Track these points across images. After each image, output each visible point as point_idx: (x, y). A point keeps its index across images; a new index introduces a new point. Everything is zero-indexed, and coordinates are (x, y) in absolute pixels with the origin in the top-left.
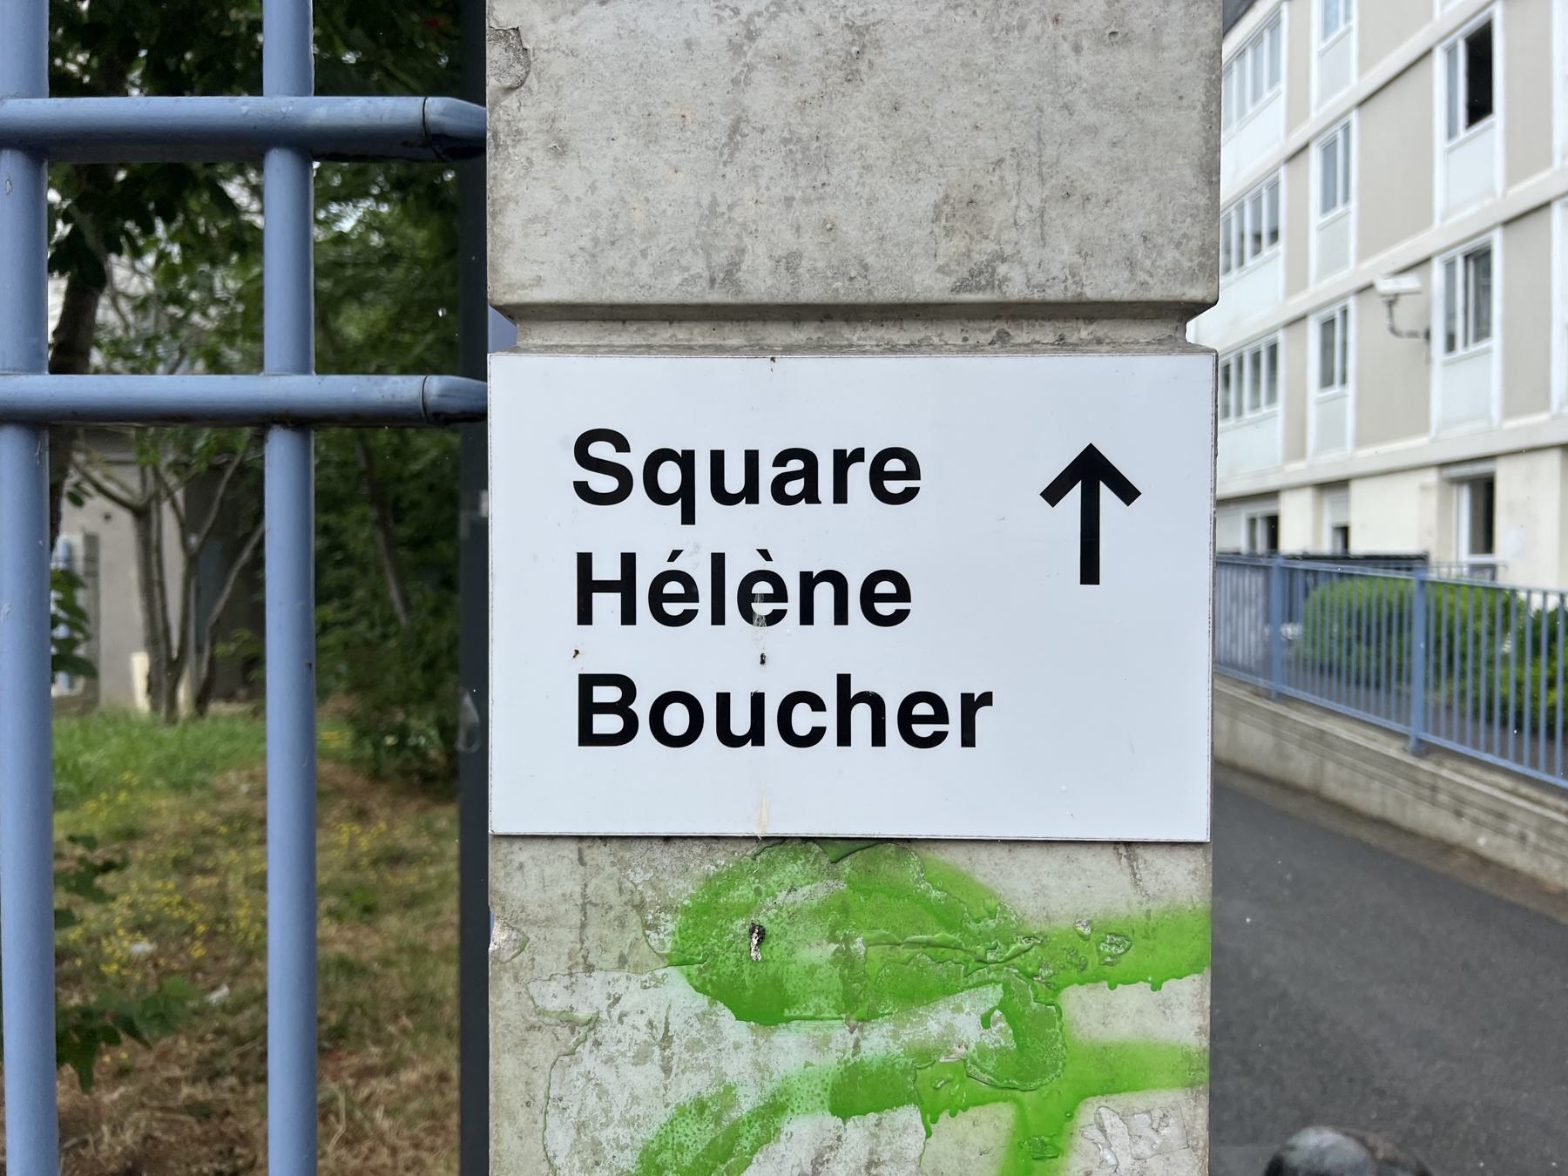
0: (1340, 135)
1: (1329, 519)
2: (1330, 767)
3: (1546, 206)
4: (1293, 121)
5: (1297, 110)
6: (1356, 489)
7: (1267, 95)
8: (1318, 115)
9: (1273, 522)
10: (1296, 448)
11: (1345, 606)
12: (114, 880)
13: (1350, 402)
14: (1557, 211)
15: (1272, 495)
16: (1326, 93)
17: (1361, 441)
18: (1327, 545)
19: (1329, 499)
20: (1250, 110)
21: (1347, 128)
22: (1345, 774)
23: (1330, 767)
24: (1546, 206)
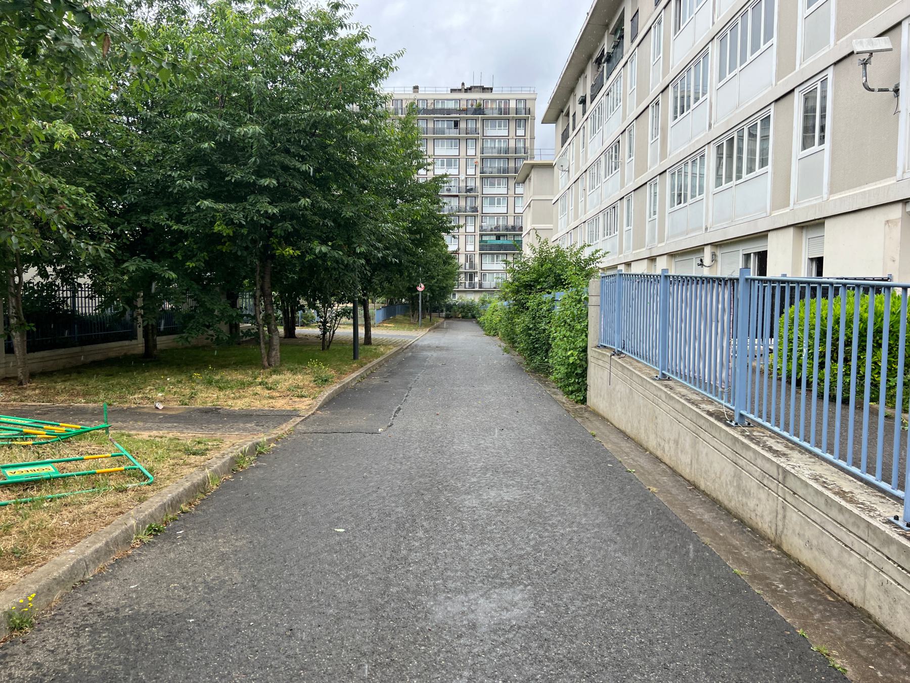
0: (819, 86)
1: (808, 252)
2: (793, 517)
3: (899, 24)
4: (781, 73)
5: (785, 65)
6: (828, 223)
7: (763, 47)
8: (804, 67)
9: (762, 257)
10: (781, 198)
11: (817, 322)
12: (82, 192)
13: (827, 155)
14: (905, 25)
15: (762, 236)
16: (810, 49)
17: (832, 192)
18: (804, 273)
19: (806, 236)
20: (750, 58)
21: (824, 81)
22: (812, 532)
23: (793, 517)
24: (899, 24)
